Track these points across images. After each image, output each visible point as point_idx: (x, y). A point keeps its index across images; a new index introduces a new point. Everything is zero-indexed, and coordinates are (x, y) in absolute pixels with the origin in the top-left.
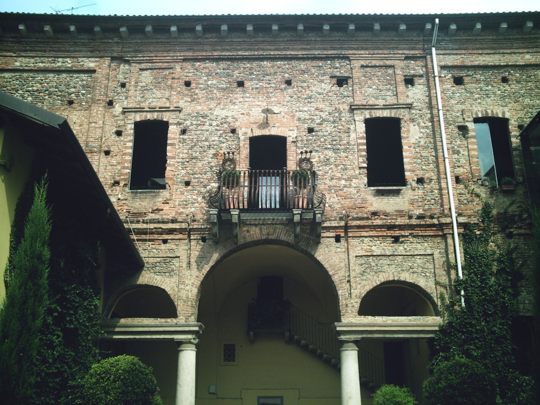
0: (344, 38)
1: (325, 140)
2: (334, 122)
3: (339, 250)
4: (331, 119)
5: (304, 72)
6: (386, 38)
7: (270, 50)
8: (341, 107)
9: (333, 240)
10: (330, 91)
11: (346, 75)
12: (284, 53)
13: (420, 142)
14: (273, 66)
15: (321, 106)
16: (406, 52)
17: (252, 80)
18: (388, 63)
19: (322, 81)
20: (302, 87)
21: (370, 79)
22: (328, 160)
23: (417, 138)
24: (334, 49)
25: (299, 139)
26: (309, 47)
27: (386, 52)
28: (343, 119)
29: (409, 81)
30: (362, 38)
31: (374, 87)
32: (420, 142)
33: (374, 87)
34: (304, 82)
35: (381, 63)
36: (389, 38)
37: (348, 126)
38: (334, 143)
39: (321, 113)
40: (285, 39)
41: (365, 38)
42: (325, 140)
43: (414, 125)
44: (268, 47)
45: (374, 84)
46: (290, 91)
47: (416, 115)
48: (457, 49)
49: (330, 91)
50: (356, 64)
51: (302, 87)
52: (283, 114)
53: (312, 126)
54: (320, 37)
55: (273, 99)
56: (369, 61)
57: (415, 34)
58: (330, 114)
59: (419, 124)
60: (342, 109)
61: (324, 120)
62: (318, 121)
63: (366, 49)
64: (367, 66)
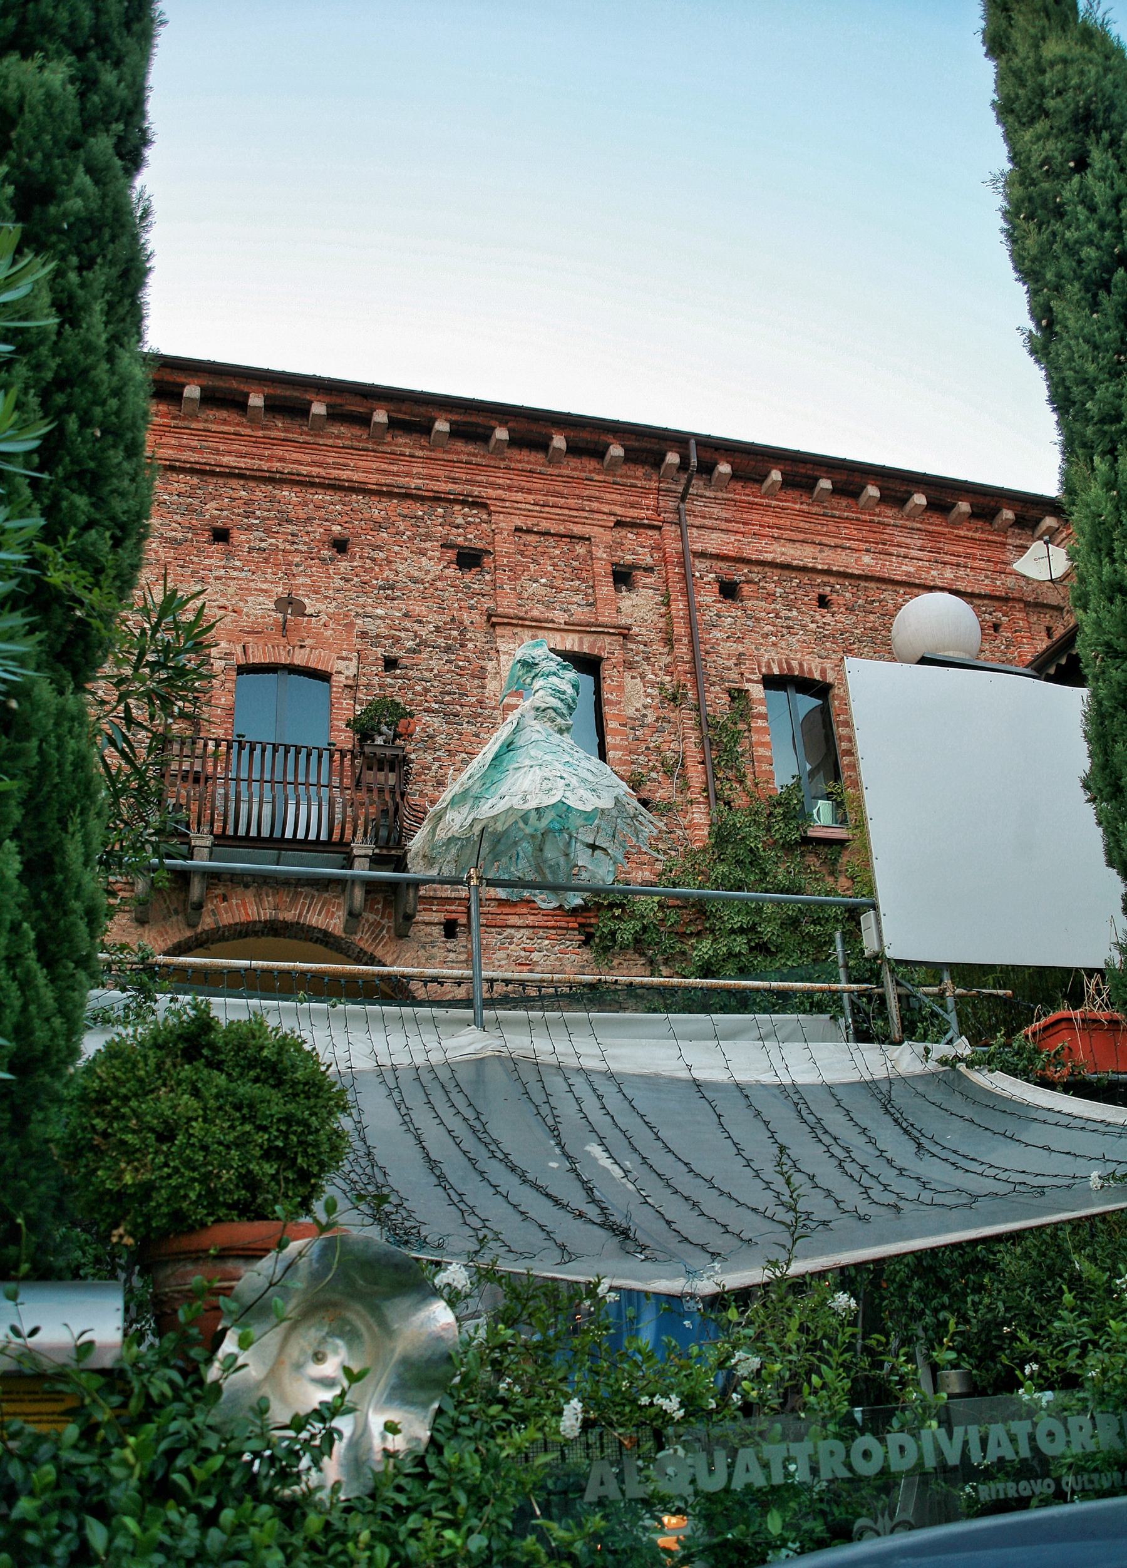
0: (478, 460)
1: (426, 690)
2: (448, 649)
3: (452, 956)
4: (441, 642)
5: (379, 526)
6: (575, 474)
7: (300, 463)
8: (466, 618)
9: (438, 931)
10: (440, 578)
11: (479, 545)
12: (335, 473)
13: (645, 716)
14: (305, 504)
15: (418, 609)
16: (619, 510)
17: (250, 528)
18: (577, 530)
19: (422, 552)
20: (373, 560)
21: (535, 561)
22: (431, 737)
23: (639, 706)
24: (455, 480)
25: (363, 680)
26: (395, 468)
27: (572, 502)
28: (470, 645)
29: (623, 577)
30: (520, 466)
31: (543, 581)
32: (645, 716)
33: (543, 581)
34: (379, 548)
35: (562, 529)
36: (583, 475)
37: (483, 663)
38: (447, 698)
39: (416, 627)
40: (340, 442)
41: (529, 467)
42: (426, 690)
43: (633, 677)
44: (295, 456)
45: (545, 574)
46: (343, 565)
47: (637, 654)
48: (727, 521)
49: (440, 578)
50: (506, 524)
51: (373, 560)
52: (324, 618)
53: (395, 652)
54: (423, 448)
55: (301, 580)
56: (535, 520)
57: (639, 474)
58: (438, 629)
59: (643, 676)
60: (467, 623)
61: (423, 643)
62: (410, 644)
63: (529, 491)
64: (529, 531)
